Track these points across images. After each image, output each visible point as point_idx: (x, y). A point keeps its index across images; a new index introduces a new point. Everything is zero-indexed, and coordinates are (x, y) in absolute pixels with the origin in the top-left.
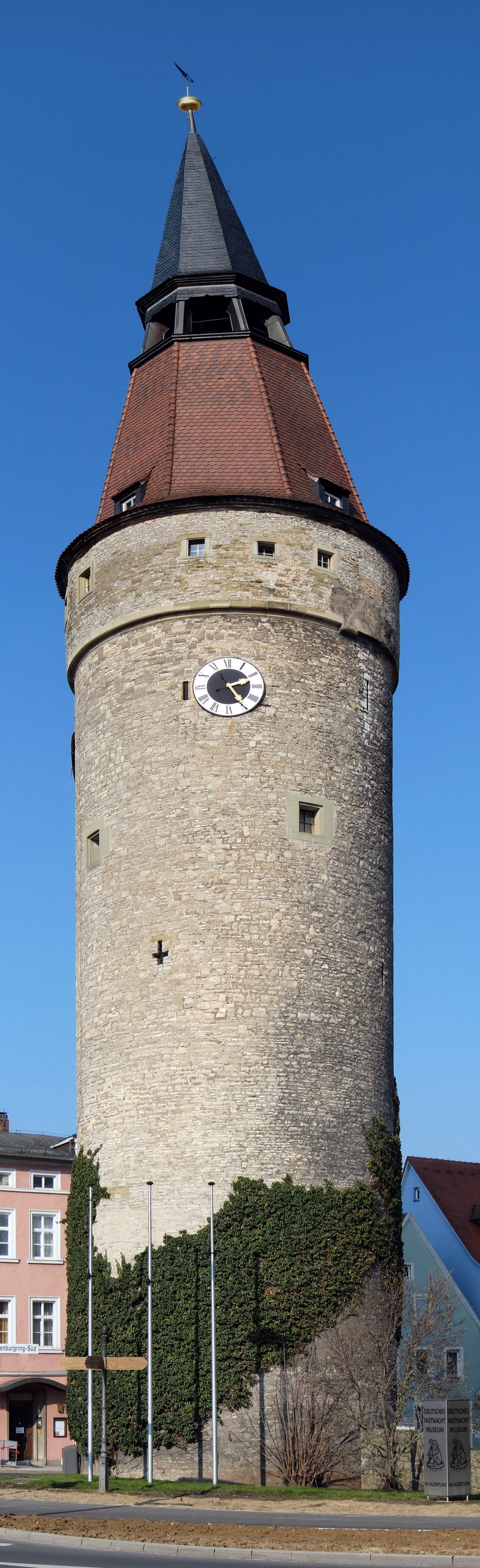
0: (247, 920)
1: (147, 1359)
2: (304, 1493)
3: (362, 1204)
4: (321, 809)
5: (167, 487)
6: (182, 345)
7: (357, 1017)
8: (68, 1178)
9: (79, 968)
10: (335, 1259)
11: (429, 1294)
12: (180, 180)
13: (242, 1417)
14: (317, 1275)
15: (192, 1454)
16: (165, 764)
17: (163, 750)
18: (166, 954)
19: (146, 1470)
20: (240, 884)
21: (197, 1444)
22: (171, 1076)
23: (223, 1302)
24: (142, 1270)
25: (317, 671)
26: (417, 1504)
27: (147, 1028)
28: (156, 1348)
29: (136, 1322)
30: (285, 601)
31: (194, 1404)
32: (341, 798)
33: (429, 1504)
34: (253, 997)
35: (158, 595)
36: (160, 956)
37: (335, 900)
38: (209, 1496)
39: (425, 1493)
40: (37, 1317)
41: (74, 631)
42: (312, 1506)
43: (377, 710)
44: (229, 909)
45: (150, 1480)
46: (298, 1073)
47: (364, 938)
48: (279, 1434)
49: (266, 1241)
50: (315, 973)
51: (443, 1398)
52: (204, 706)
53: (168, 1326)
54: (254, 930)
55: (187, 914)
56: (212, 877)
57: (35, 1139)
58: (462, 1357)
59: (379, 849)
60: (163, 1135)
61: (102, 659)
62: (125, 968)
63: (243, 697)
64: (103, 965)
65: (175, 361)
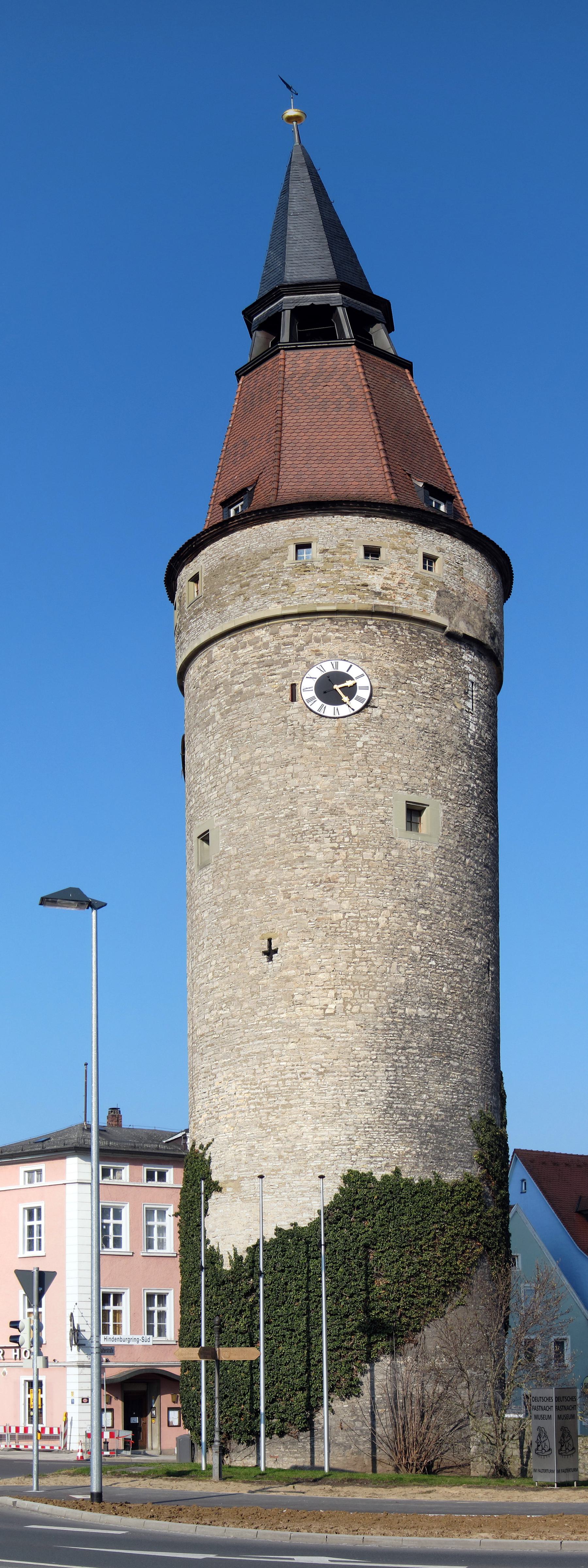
0: (356, 917)
1: (259, 1349)
2: (415, 1480)
3: (470, 1196)
4: (427, 808)
5: (274, 493)
6: (289, 353)
7: (464, 1013)
8: (181, 1171)
10: (443, 1250)
11: (537, 1284)
12: (285, 191)
14: (426, 1266)
15: (304, 1443)
16: (274, 764)
17: (271, 751)
18: (276, 951)
19: (258, 1459)
20: (348, 882)
21: (309, 1432)
22: (281, 1072)
23: (334, 1293)
24: (253, 1262)
25: (422, 672)
28: (268, 1339)
29: (248, 1313)
31: (305, 1394)
32: (447, 797)
33: (538, 1490)
34: (362, 993)
36: (270, 953)
37: (442, 898)
38: (321, 1484)
39: (534, 1480)
40: (151, 1309)
41: (183, 635)
42: (422, 1493)
43: (482, 711)
44: (338, 907)
45: (262, 1469)
46: (406, 1067)
47: (471, 934)
48: (389, 1423)
49: (375, 1232)
50: (423, 970)
52: (311, 707)
53: (279, 1317)
54: (362, 927)
55: (297, 912)
56: (321, 876)
57: (147, 1134)
58: (569, 1346)
59: (485, 847)
60: (274, 1129)
61: (211, 662)
62: (236, 966)
63: (350, 699)
64: (214, 963)
65: (281, 369)
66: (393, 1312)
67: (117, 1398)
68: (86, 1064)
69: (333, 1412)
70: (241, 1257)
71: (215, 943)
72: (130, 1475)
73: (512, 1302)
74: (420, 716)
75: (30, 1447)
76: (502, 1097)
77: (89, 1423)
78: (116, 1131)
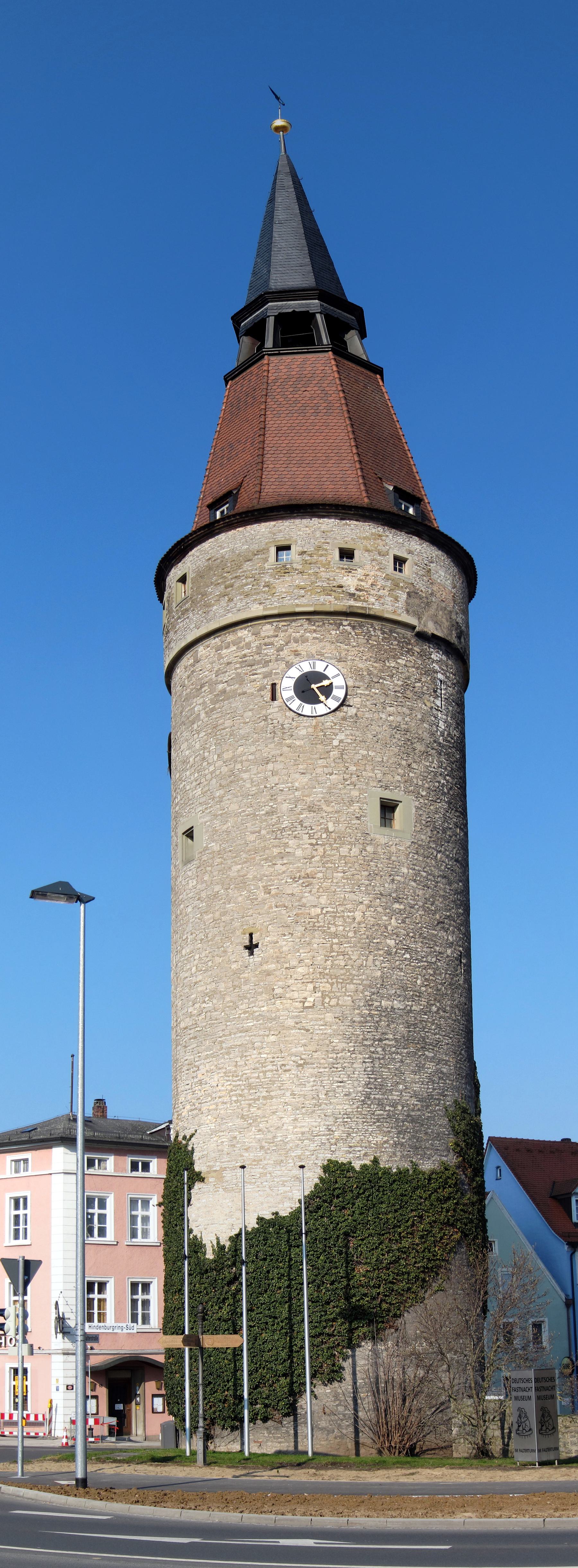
0: (333, 912)
1: (242, 1336)
2: (398, 1462)
3: (446, 1183)
4: (400, 804)
5: (257, 496)
6: (272, 358)
7: (438, 1004)
8: (164, 1162)
9: (174, 959)
10: (422, 1237)
11: (514, 1268)
12: (272, 200)
13: (336, 1391)
14: (405, 1253)
15: (287, 1428)
16: (255, 762)
18: (257, 946)
19: (243, 1444)
20: (325, 878)
21: (292, 1418)
22: (262, 1064)
23: (315, 1280)
24: (236, 1250)
26: (508, 1470)
27: (239, 1017)
28: (251, 1326)
29: (231, 1301)
30: (365, 605)
31: (288, 1380)
32: (419, 793)
33: (519, 1470)
34: (340, 986)
35: (248, 600)
36: (251, 947)
37: (415, 892)
38: (305, 1468)
39: (515, 1459)
40: (135, 1297)
41: (171, 634)
42: (406, 1475)
43: (451, 708)
44: (316, 902)
45: (247, 1454)
46: (383, 1058)
47: (443, 928)
48: (371, 1407)
49: (355, 1221)
50: (398, 963)
51: (530, 1367)
52: (290, 706)
53: (262, 1304)
54: (339, 922)
55: (277, 907)
56: (300, 871)
57: (132, 1125)
58: (547, 1328)
59: (455, 842)
60: (255, 1120)
61: (197, 661)
63: (327, 698)
64: (197, 957)
65: (265, 374)
66: (374, 1299)
67: (101, 1385)
68: (73, 1056)
69: (316, 1397)
70: (224, 1246)
71: (199, 937)
72: (115, 1461)
73: (490, 1286)
74: (393, 715)
75: (15, 1433)
76: (476, 1086)
77: (74, 1409)
78: (101, 1122)
